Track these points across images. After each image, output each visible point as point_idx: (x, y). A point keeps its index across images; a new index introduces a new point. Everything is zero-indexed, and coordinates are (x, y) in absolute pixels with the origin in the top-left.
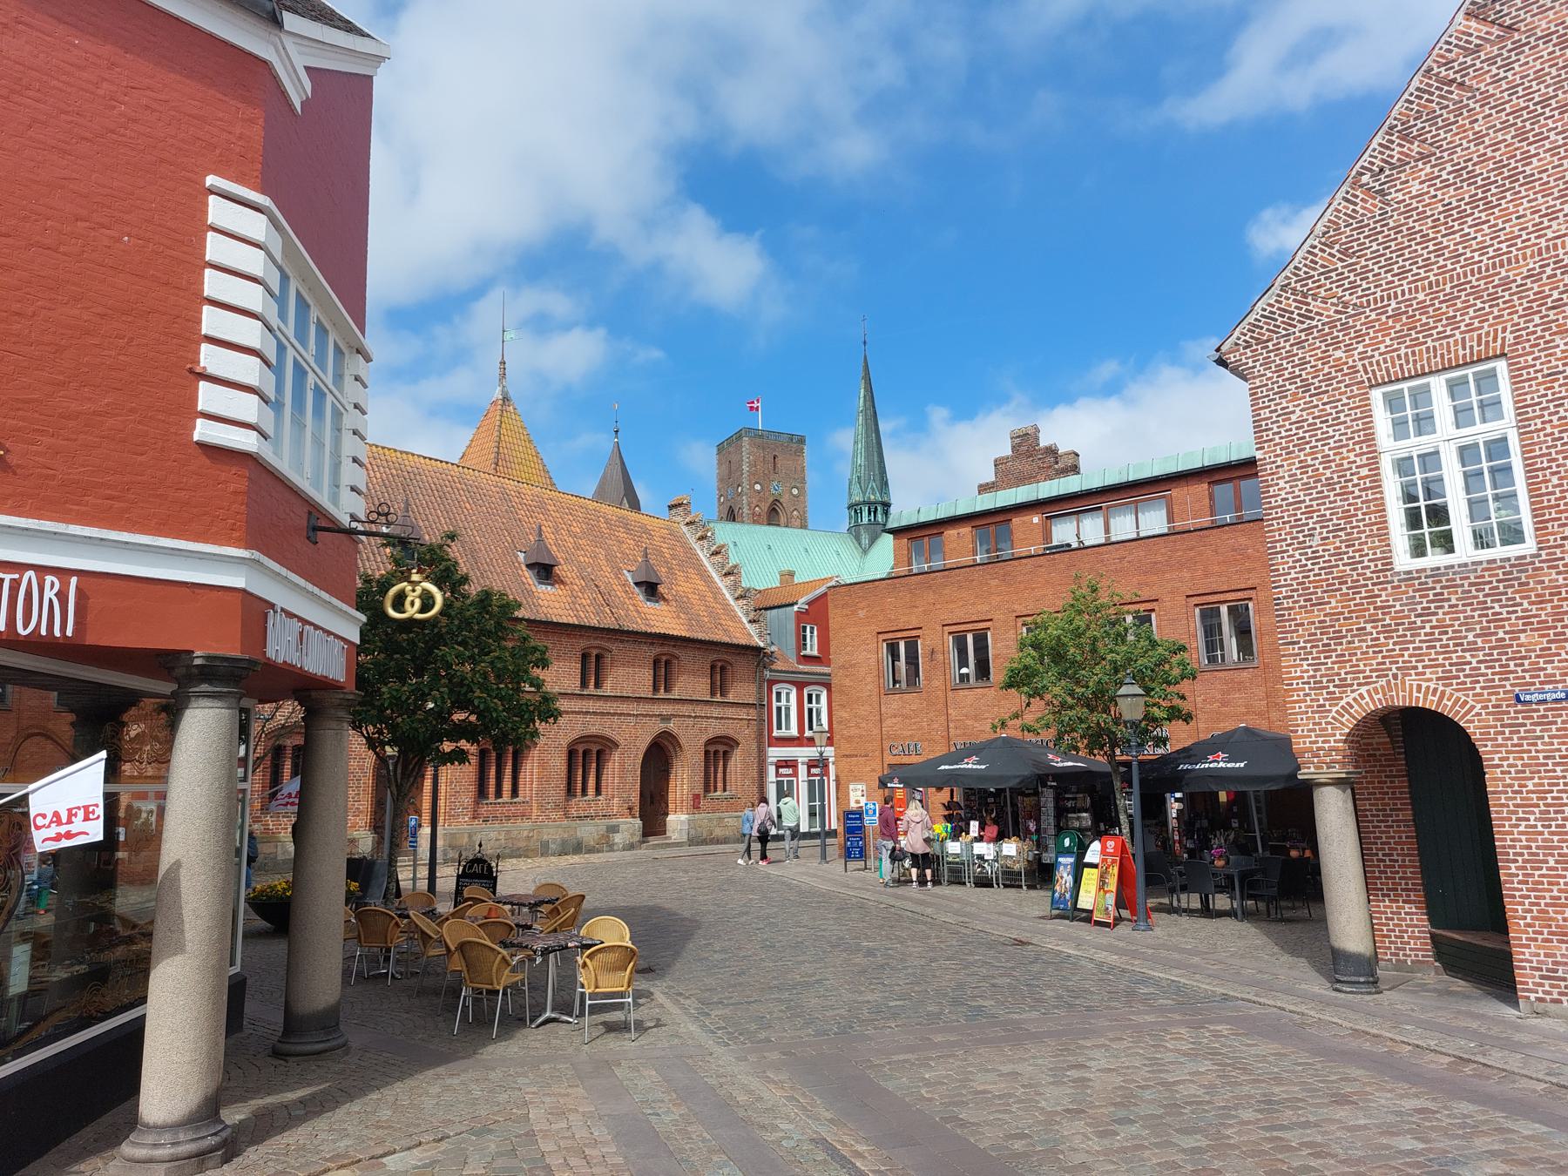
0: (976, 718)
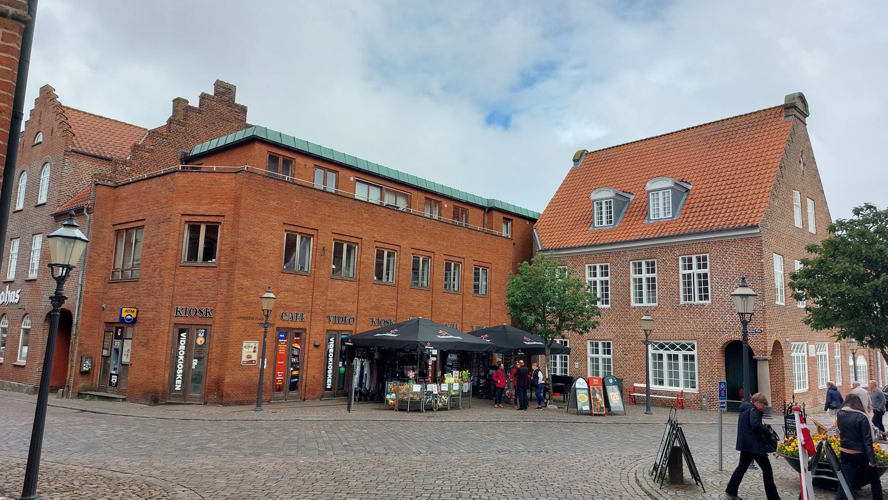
0: (344, 300)
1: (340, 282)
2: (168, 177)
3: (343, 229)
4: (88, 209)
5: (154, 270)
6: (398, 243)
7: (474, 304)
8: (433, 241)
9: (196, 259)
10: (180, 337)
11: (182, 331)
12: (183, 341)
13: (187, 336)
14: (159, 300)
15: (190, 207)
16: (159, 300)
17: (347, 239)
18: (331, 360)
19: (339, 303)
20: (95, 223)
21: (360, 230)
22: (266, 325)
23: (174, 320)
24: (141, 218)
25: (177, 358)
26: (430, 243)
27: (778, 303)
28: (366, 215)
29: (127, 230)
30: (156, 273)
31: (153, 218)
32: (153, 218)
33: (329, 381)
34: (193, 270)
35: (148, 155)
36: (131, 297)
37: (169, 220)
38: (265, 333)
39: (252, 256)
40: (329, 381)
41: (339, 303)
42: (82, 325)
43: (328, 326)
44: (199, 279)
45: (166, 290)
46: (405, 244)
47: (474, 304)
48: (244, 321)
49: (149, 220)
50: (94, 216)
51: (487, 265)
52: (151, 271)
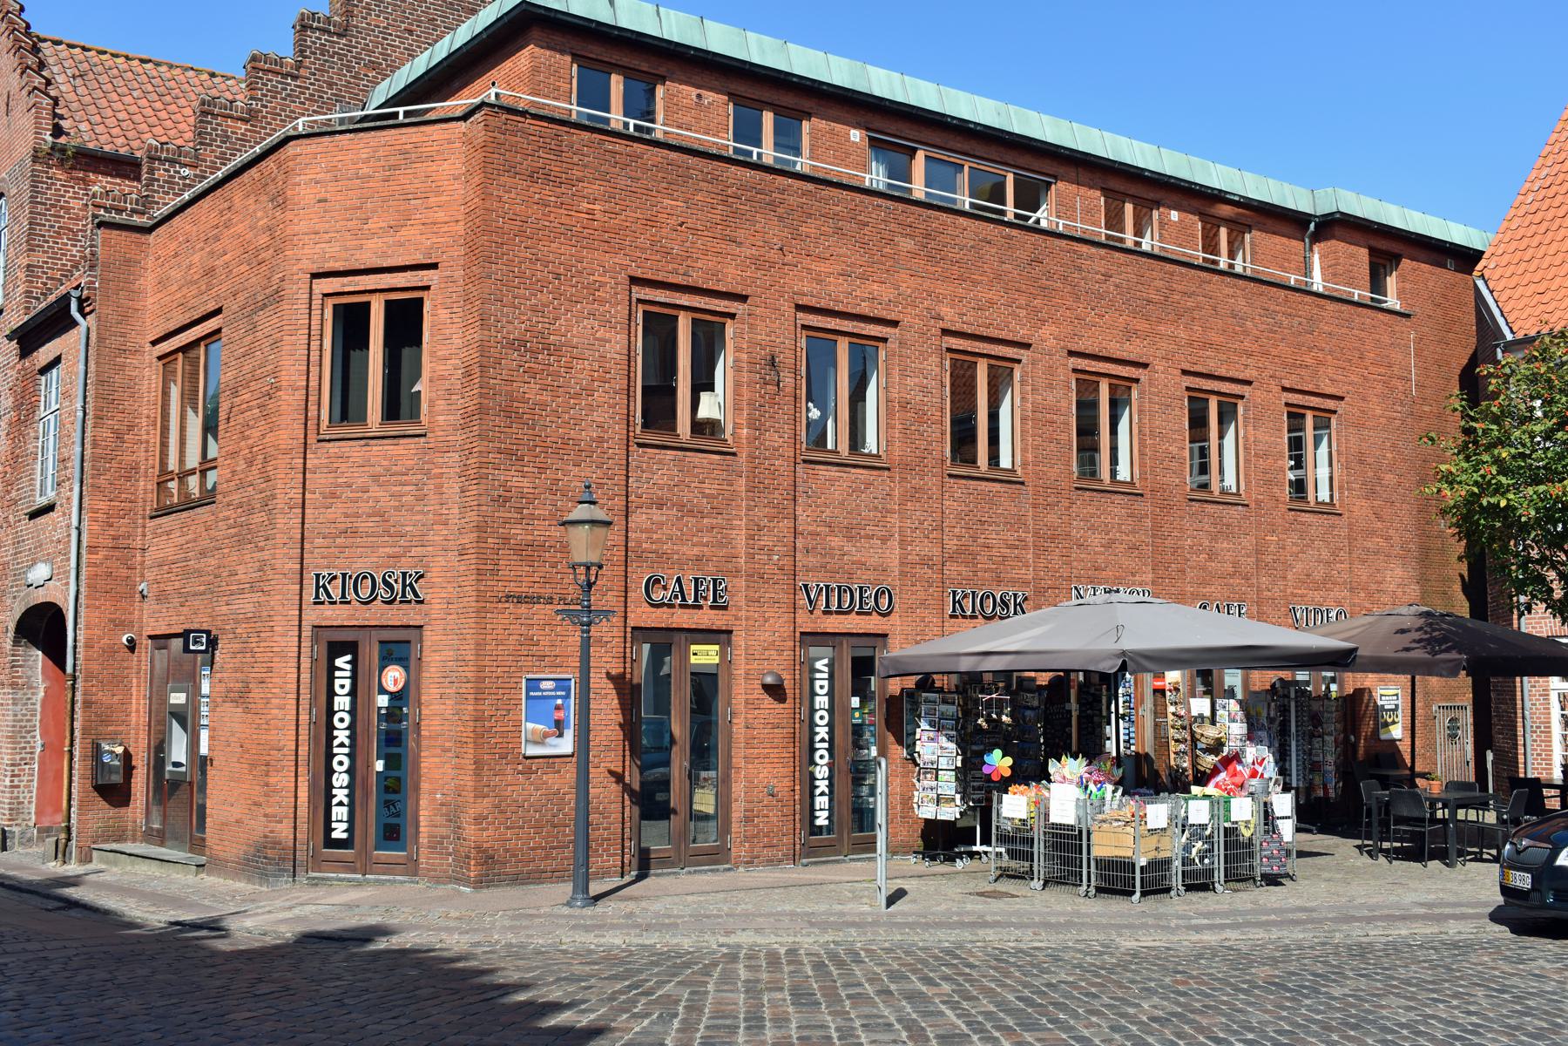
0: (850, 532)
1: (833, 472)
2: (269, 164)
3: (836, 292)
4: (81, 301)
5: (250, 463)
6: (1021, 334)
7: (1295, 537)
8: (1141, 325)
9: (362, 418)
10: (332, 669)
11: (335, 649)
12: (342, 683)
13: (354, 663)
14: (266, 555)
15: (333, 249)
16: (266, 555)
17: (848, 326)
18: (342, 736)
19: (836, 541)
20: (100, 339)
21: (886, 293)
22: (585, 616)
23: (313, 616)
24: (211, 307)
25: (813, 734)
26: (1129, 334)
27: (997, 753)
28: (907, 244)
29: (185, 349)
30: (255, 470)
31: (241, 298)
32: (241, 298)
33: (822, 802)
34: (354, 450)
35: (243, 127)
36: (203, 554)
37: (277, 297)
38: (586, 644)
39: (532, 391)
40: (822, 802)
41: (836, 541)
42: (88, 646)
43: (806, 623)
44: (375, 477)
45: (281, 521)
46: (1047, 337)
47: (1295, 537)
48: (523, 609)
49: (232, 307)
50: (99, 319)
51: (1330, 404)
52: (242, 466)
